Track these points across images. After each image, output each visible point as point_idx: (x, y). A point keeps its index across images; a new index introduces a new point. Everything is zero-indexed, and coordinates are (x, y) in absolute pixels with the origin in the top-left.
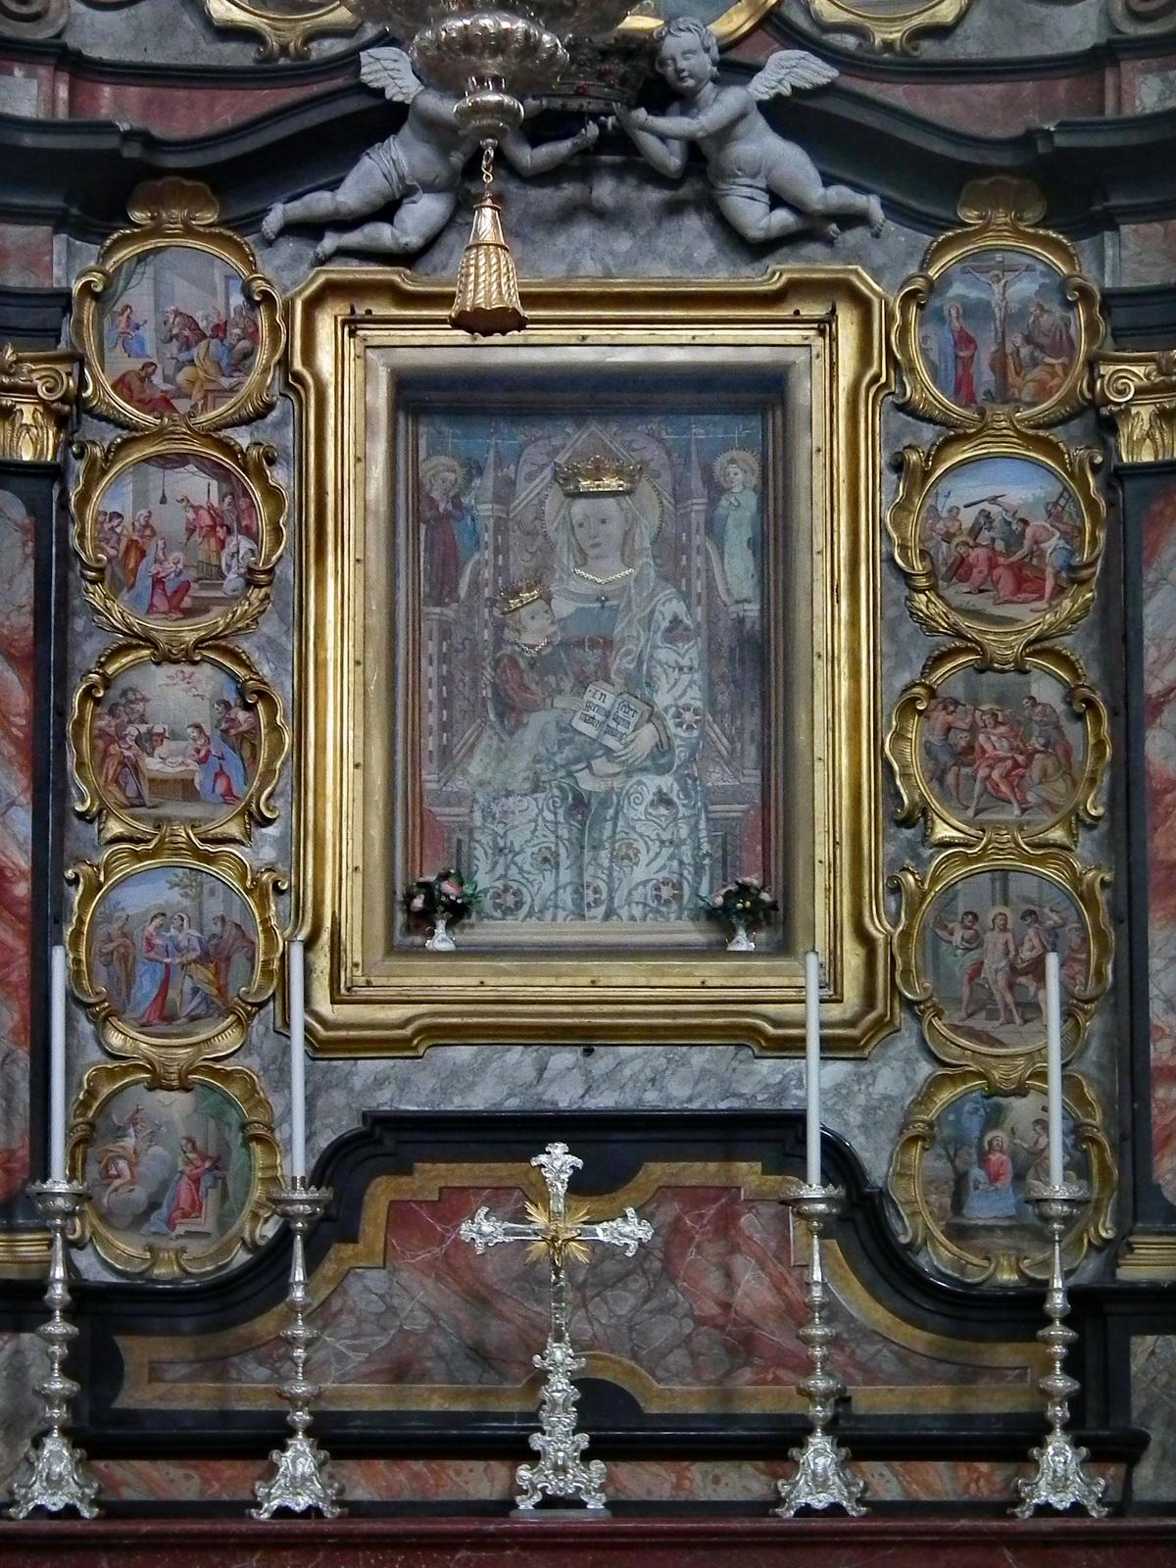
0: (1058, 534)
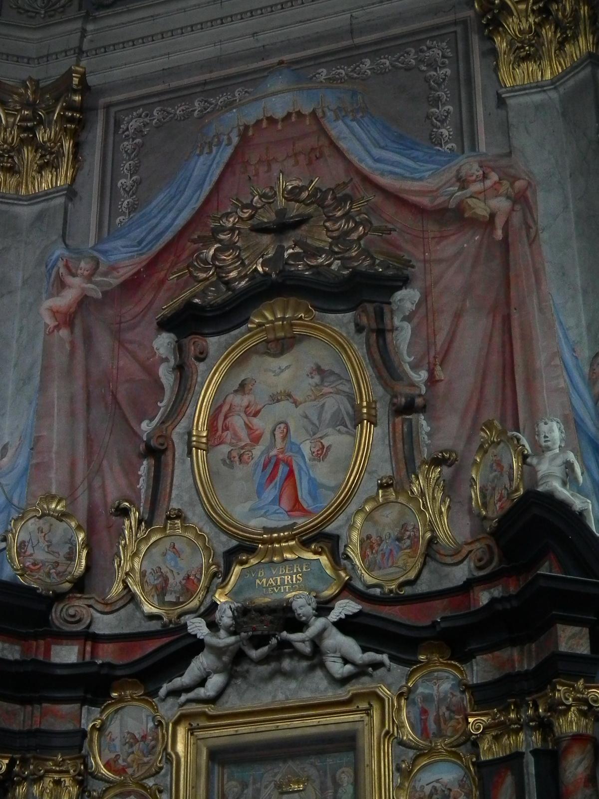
0: (463, 794)
